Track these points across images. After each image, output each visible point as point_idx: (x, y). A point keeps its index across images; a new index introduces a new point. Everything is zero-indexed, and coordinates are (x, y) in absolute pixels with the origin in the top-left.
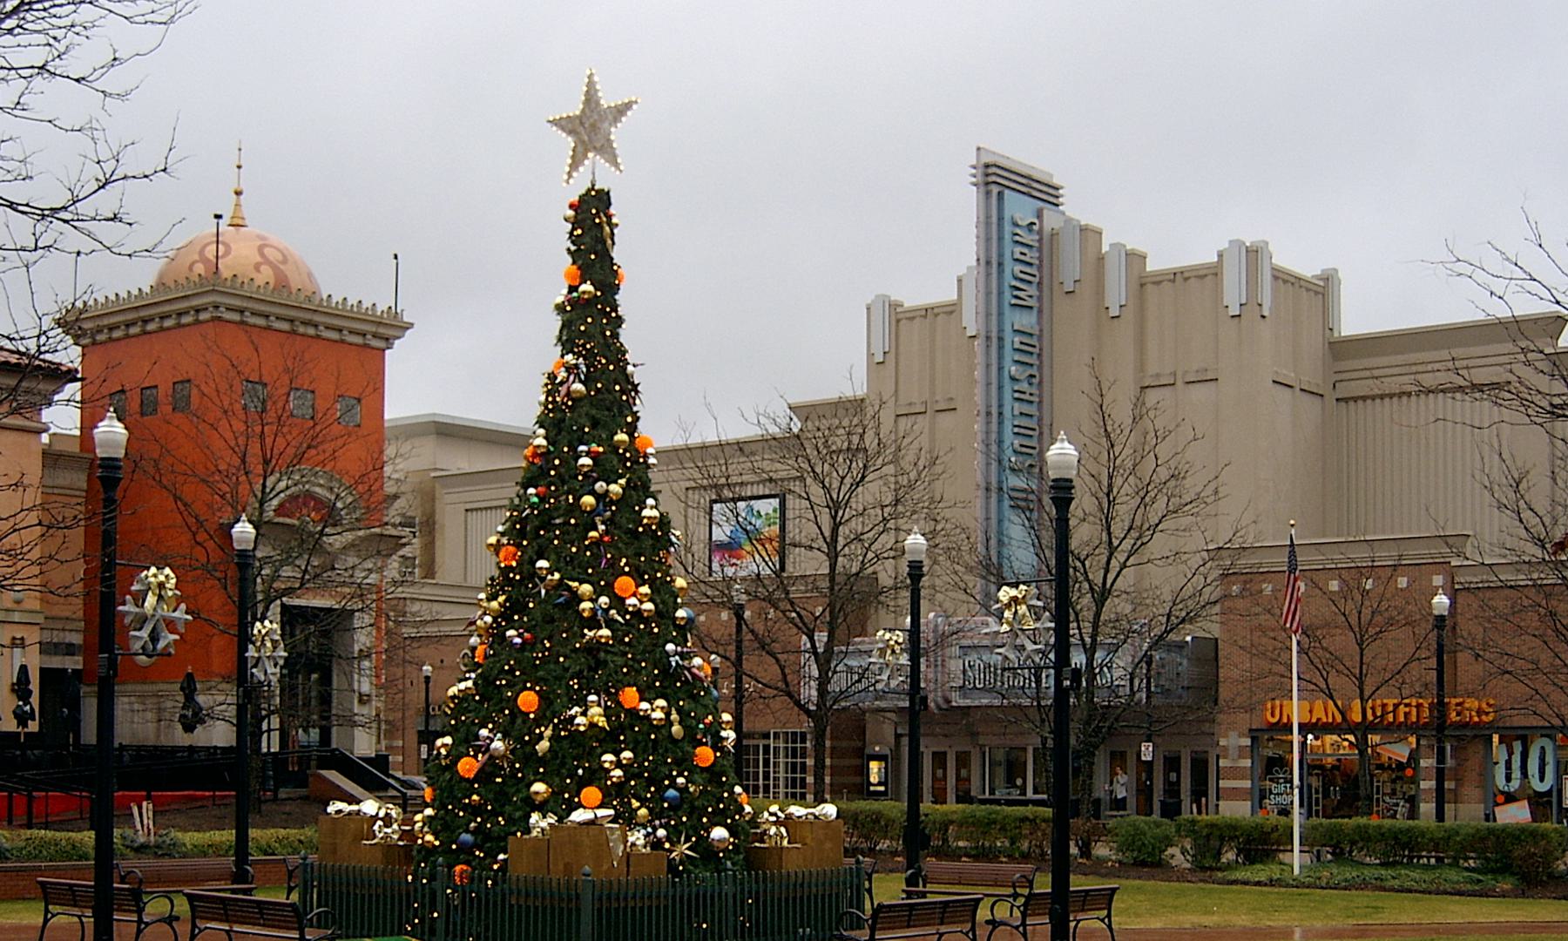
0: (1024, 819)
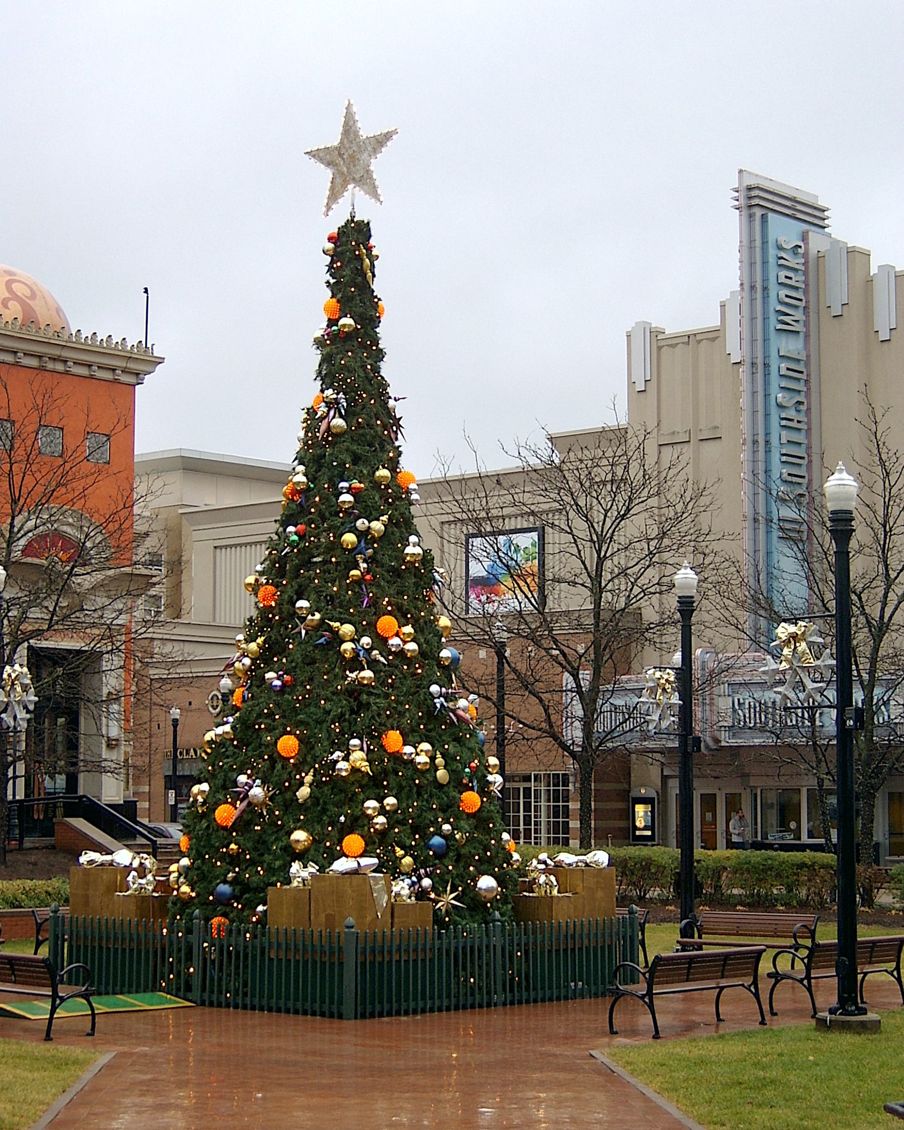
0: (802, 865)
